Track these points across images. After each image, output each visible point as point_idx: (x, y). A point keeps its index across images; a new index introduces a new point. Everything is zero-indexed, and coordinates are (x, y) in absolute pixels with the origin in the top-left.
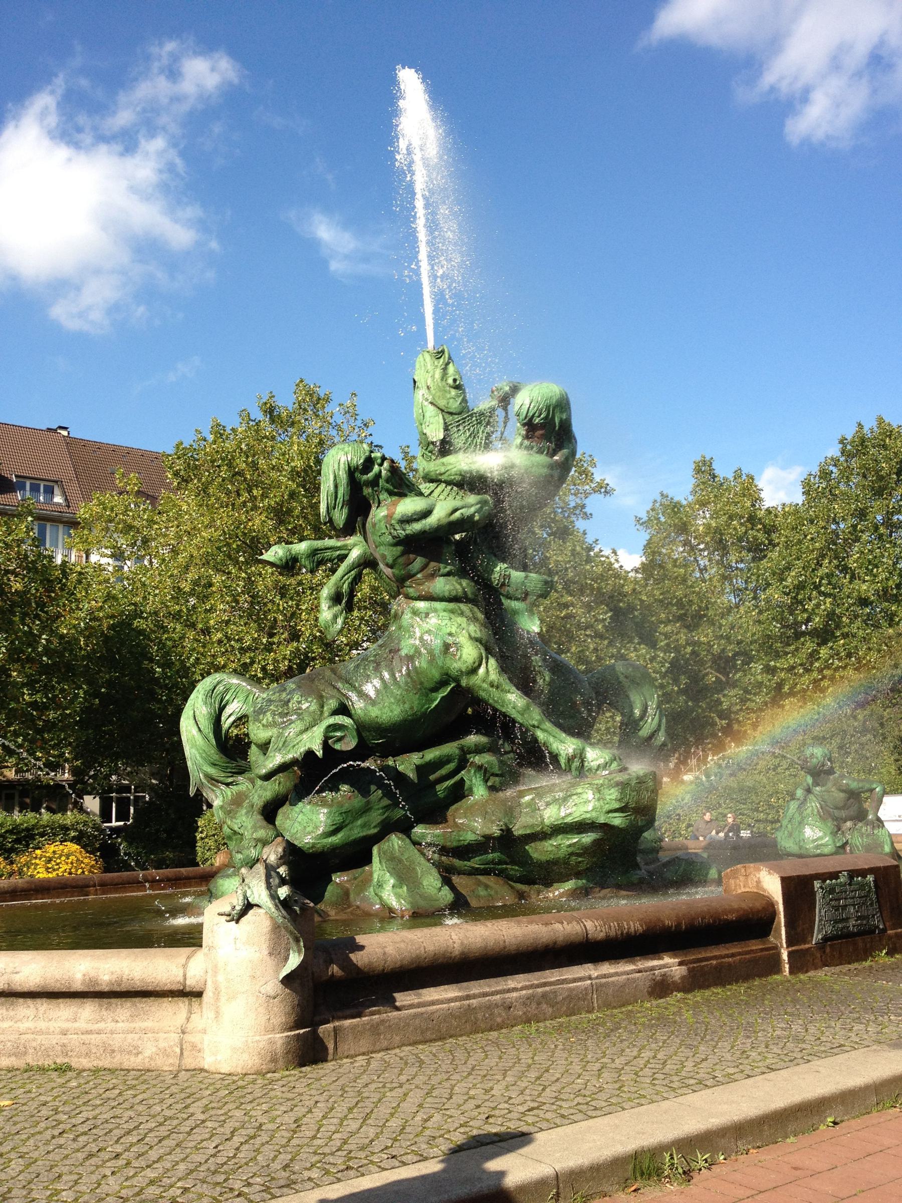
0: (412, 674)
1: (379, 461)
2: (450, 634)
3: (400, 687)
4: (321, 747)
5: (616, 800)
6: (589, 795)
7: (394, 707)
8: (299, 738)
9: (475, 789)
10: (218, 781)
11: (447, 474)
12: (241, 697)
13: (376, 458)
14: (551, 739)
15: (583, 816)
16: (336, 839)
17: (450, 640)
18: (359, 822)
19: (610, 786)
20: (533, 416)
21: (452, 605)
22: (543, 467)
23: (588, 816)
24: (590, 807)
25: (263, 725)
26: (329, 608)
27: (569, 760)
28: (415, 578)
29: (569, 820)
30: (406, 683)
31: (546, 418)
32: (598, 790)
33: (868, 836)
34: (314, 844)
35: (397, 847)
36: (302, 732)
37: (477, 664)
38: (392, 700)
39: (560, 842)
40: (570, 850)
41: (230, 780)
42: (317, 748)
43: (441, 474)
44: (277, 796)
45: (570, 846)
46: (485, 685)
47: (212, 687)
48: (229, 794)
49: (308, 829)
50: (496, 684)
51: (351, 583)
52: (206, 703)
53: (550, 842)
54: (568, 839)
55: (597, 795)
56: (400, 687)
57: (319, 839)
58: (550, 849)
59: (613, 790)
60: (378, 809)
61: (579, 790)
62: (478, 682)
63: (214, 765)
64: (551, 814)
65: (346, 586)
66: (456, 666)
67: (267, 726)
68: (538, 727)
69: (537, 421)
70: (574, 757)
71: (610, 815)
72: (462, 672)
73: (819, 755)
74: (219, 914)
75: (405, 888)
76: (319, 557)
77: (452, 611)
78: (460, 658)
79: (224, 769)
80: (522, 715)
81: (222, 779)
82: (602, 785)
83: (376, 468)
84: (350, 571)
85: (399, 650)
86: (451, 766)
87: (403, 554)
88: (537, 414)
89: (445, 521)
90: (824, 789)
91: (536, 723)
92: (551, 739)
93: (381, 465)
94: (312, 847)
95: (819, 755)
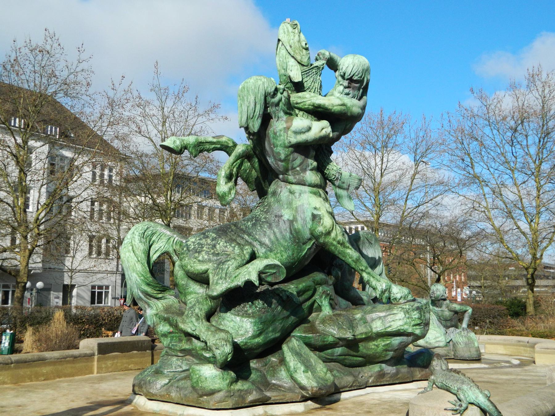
0: (293, 232)
1: (281, 91)
2: (315, 208)
3: (286, 241)
4: (257, 278)
5: (418, 318)
6: (401, 315)
7: (283, 253)
8: (238, 271)
9: (323, 308)
10: (151, 296)
11: (302, 104)
12: (164, 240)
13: (280, 89)
14: (372, 279)
15: (399, 328)
16: (259, 340)
17: (316, 212)
18: (271, 329)
19: (413, 310)
20: (353, 75)
21: (315, 189)
22: (359, 107)
23: (402, 328)
24: (401, 323)
25: (199, 261)
26: (226, 183)
27: (382, 292)
28: (295, 170)
29: (389, 330)
30: (290, 238)
31: (361, 77)
32: (407, 312)
33: (465, 336)
34: (246, 343)
35: (296, 345)
36: (238, 267)
37: (331, 229)
38: (282, 249)
39: (379, 343)
40: (384, 348)
41: (160, 296)
42: (255, 279)
43: (297, 103)
44: (211, 309)
45: (384, 346)
46: (335, 243)
47: (143, 231)
48: (160, 305)
49: (241, 332)
50: (341, 242)
51: (238, 168)
52: (141, 242)
53: (374, 343)
54: (384, 341)
55: (407, 316)
56: (286, 241)
57: (250, 339)
58: (373, 347)
59: (415, 312)
60: (279, 320)
61: (395, 312)
62: (331, 240)
63: (148, 285)
64: (378, 327)
65: (235, 170)
66: (320, 229)
67: (202, 261)
68: (364, 271)
69: (355, 78)
70: (385, 290)
71: (414, 327)
72: (322, 233)
73: (441, 290)
74: (445, 409)
75: (310, 373)
76: (202, 147)
77: (315, 193)
78: (323, 224)
79: (154, 288)
80: (356, 262)
81: (155, 295)
82: (409, 309)
83: (279, 95)
84: (237, 160)
85: (282, 216)
86: (310, 293)
87: (292, 153)
88: (356, 74)
89: (318, 136)
90: (440, 309)
91: (364, 269)
92: (372, 279)
93: (282, 94)
94: (245, 345)
95: (441, 290)
